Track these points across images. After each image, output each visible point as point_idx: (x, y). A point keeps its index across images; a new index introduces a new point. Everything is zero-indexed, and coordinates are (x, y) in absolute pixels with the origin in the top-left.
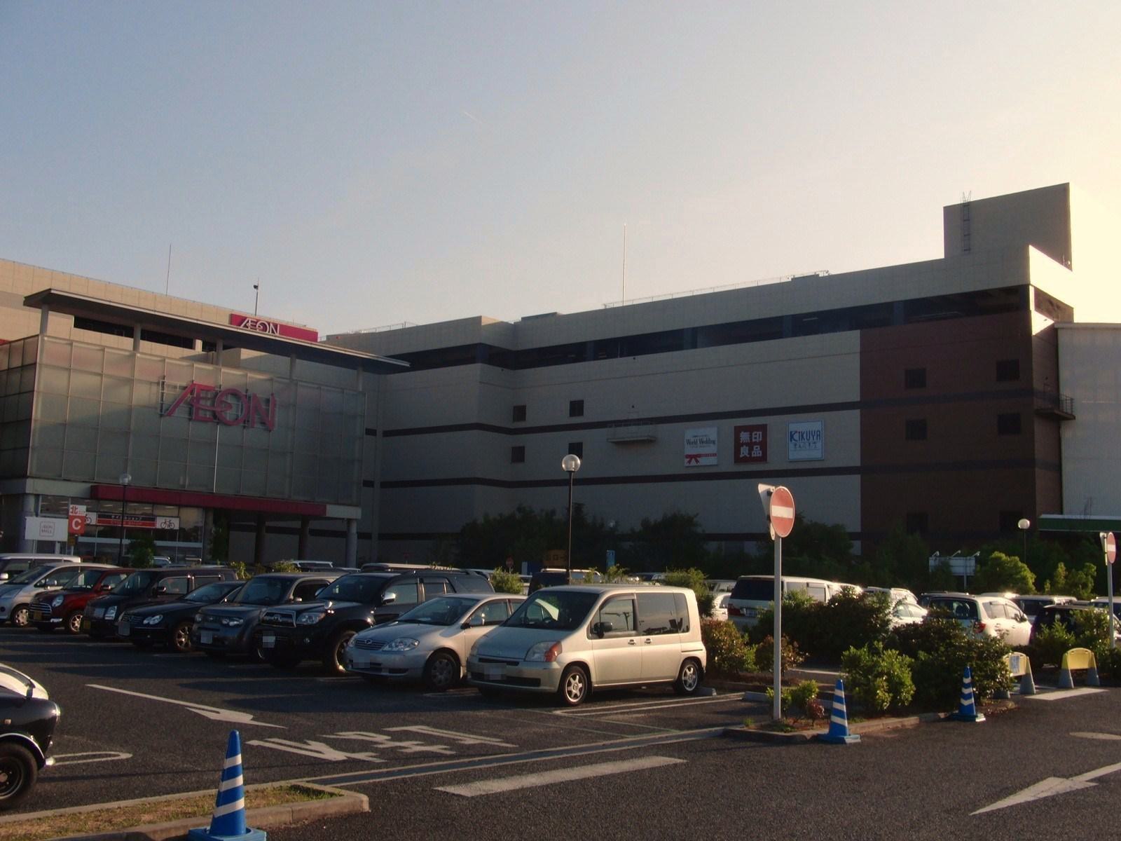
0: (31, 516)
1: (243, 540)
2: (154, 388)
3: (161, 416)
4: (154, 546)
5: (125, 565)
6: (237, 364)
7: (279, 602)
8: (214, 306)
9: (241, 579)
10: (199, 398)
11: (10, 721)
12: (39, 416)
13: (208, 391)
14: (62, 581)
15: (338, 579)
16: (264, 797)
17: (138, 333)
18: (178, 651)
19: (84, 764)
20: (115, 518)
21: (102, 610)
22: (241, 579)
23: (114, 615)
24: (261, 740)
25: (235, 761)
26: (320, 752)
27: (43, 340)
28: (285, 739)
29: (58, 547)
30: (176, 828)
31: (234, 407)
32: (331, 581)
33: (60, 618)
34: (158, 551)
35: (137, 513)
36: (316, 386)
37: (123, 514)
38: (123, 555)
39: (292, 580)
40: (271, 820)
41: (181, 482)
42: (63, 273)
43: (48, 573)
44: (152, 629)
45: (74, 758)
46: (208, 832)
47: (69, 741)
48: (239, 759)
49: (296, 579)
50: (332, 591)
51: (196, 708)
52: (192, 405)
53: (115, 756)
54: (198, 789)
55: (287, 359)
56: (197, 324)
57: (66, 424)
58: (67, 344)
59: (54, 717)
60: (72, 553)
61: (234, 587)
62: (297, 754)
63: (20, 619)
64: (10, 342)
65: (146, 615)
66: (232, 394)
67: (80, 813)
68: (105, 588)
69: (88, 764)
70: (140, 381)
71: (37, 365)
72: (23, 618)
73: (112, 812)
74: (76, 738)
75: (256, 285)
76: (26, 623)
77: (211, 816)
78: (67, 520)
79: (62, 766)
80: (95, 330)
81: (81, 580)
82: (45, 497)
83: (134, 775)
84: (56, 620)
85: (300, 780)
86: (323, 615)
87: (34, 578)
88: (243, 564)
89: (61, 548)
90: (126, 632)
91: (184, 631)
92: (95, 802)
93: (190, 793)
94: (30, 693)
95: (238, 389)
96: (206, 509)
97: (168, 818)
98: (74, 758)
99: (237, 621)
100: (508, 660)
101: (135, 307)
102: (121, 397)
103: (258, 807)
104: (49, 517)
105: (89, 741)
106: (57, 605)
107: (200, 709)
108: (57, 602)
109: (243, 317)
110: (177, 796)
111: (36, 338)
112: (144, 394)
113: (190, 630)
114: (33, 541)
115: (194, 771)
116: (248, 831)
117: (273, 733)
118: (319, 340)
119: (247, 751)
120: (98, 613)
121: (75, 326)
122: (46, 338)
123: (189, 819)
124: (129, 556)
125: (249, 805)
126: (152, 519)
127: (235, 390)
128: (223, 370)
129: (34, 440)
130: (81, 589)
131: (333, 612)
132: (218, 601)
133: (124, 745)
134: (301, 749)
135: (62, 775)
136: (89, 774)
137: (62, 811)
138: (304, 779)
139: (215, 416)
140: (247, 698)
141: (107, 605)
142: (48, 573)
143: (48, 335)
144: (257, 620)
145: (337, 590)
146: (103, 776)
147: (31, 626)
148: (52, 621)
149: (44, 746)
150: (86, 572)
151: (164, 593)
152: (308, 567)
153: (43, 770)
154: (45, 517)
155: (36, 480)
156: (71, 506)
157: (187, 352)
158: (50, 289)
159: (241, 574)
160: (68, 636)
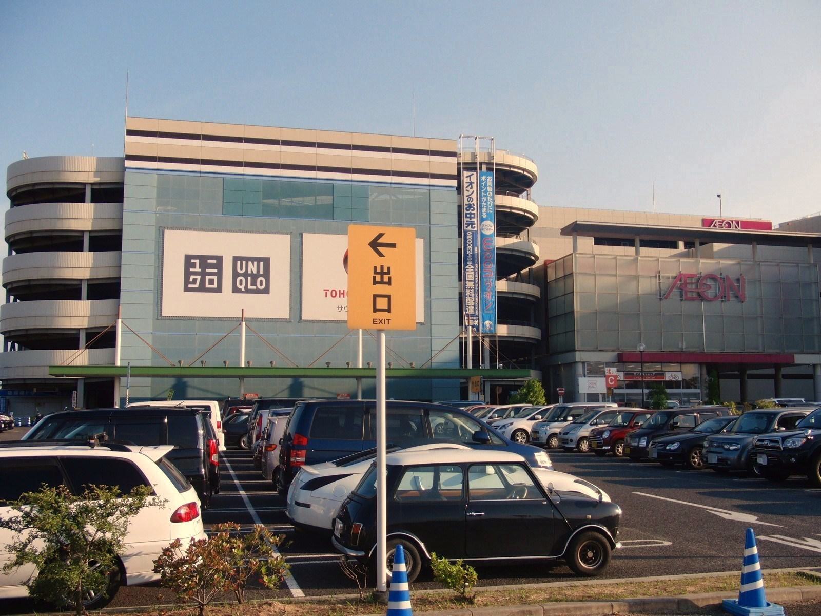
0: (582, 377)
1: (730, 386)
2: (654, 281)
3: (661, 299)
4: (665, 393)
5: (648, 408)
6: (711, 255)
7: (766, 431)
8: (689, 215)
9: (734, 415)
10: (686, 284)
11: (590, 517)
12: (579, 309)
13: (692, 277)
14: (607, 421)
15: (813, 412)
16: (777, 580)
17: (638, 242)
18: (694, 468)
19: (640, 548)
20: (636, 375)
21: (637, 440)
22: (734, 415)
23: (645, 443)
24: (767, 536)
25: (752, 551)
26: (817, 548)
27: (576, 257)
28: (786, 536)
29: (600, 396)
30: (713, 598)
31: (713, 287)
32: (808, 413)
33: (609, 446)
34: (670, 397)
35: (651, 370)
36: (776, 264)
37: (642, 371)
38: (645, 401)
39: (775, 414)
40: (785, 598)
41: (680, 346)
42: (583, 209)
43: (597, 416)
44: (673, 453)
45: (632, 544)
46: (737, 603)
47: (627, 531)
48: (755, 550)
49: (778, 413)
50: (809, 420)
51: (713, 510)
52: (682, 289)
53: (660, 543)
54: (724, 570)
55: (751, 246)
56: (649, 228)
57: (638, 315)
58: (775, 265)
59: (618, 515)
60: (611, 401)
61: (730, 420)
62: (798, 548)
63: (583, 447)
64: (555, 261)
65: (667, 443)
66: (710, 278)
67: (643, 582)
68: (636, 424)
69: (643, 548)
70: (643, 277)
71: (574, 274)
72: (585, 446)
73: (665, 583)
74: (632, 530)
75: (719, 194)
76: (587, 450)
77: (739, 592)
78: (605, 378)
79: (625, 548)
80: (608, 245)
81: (619, 420)
82: (589, 363)
83: (676, 557)
84: (606, 448)
85: (804, 568)
86: (804, 440)
87: (589, 419)
88: (734, 403)
89: (603, 398)
90: (655, 455)
91: (696, 453)
92: (651, 575)
93: (718, 573)
94: (601, 498)
95: (713, 273)
96: (701, 364)
97: (706, 591)
98: (632, 544)
99: (735, 446)
100: (369, 456)
101: (665, 226)
102: (631, 289)
103: (773, 587)
104: (592, 377)
105: (641, 532)
106: (606, 437)
107: (716, 511)
108: (606, 435)
109: (710, 220)
110: (709, 574)
111: (571, 256)
112: (647, 286)
113: (700, 453)
114: (584, 394)
115: (719, 557)
116: (768, 605)
117: (775, 531)
118: (773, 228)
119: (759, 543)
120: (634, 442)
121: (595, 244)
122: (577, 255)
123: (722, 592)
124: (649, 401)
125: (766, 585)
126: (662, 374)
127: (712, 275)
128: (702, 261)
129: (577, 326)
130: (620, 426)
131: (812, 438)
132: (719, 432)
133: (665, 536)
134: (800, 544)
135: (627, 555)
136: (644, 555)
137: (630, 579)
138: (807, 568)
139: (699, 295)
140: (751, 504)
141: (639, 436)
142: (597, 416)
143: (578, 252)
144: (751, 445)
145: (813, 420)
146: (654, 557)
147: (590, 452)
148: (604, 448)
149: (614, 534)
150: (622, 413)
151: (678, 427)
152: (785, 403)
153: (614, 550)
154: (589, 377)
155: (581, 352)
156: (606, 368)
157: (673, 251)
158: (576, 221)
159: (733, 412)
160: (615, 458)
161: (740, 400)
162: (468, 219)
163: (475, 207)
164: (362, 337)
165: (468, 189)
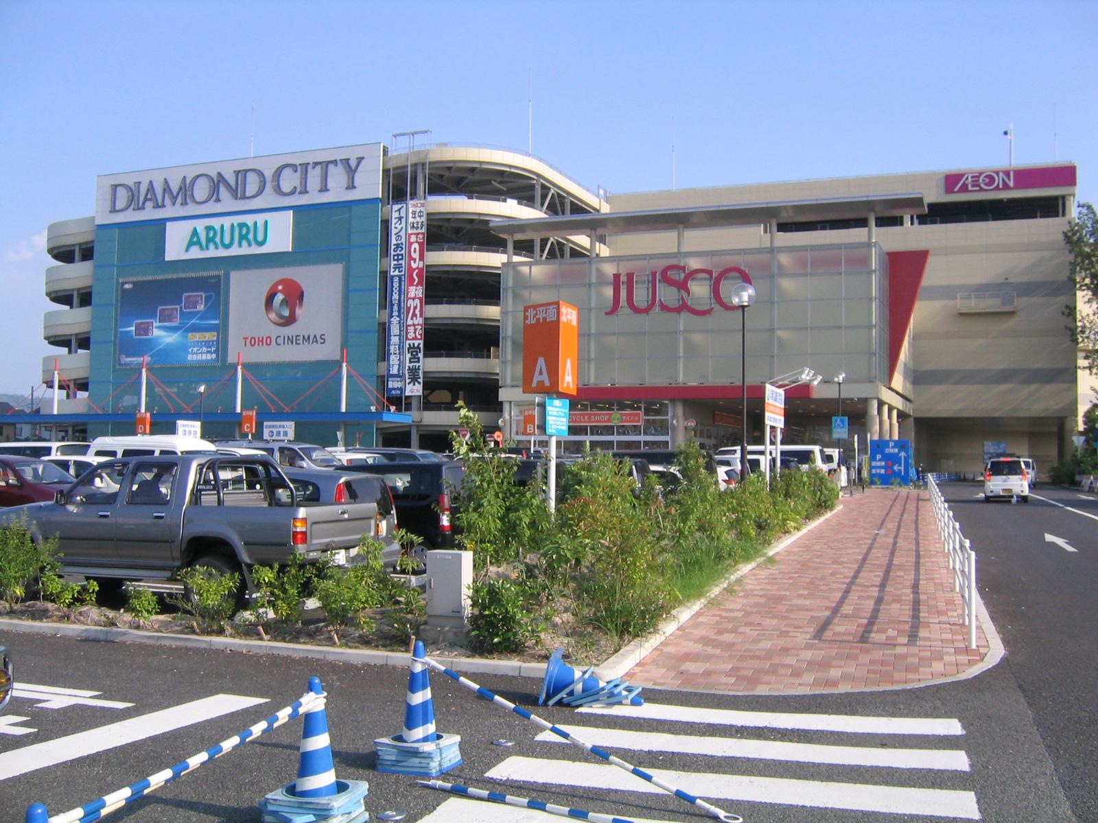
161: (548, 408)
162: (396, 262)
163: (404, 246)
164: (976, 633)
165: (397, 225)
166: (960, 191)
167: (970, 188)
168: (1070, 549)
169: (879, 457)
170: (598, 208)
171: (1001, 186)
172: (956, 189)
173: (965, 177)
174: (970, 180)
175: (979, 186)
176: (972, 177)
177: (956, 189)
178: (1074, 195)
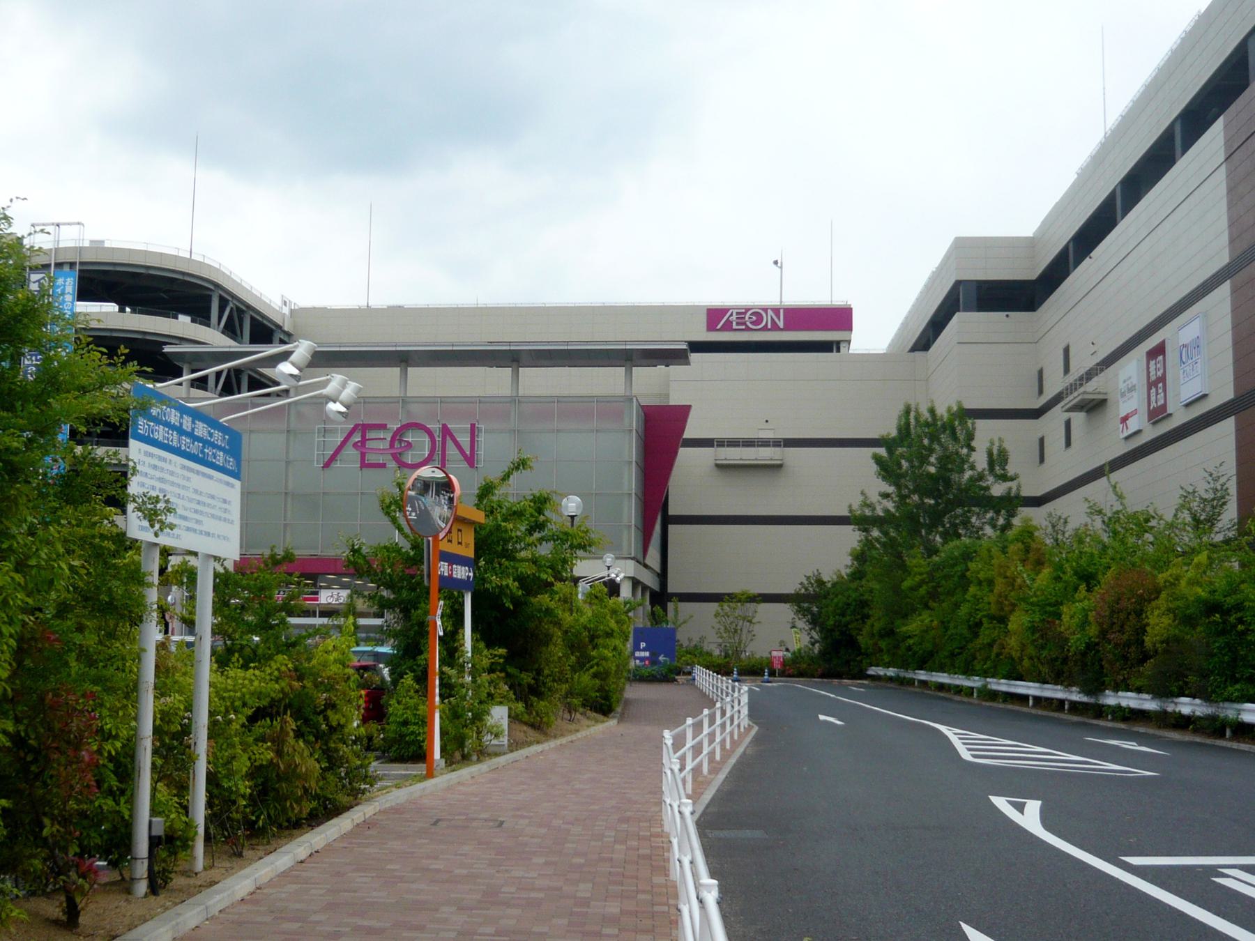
166: (723, 329)
167: (735, 326)
168: (839, 723)
169: (643, 645)
170: (281, 324)
171: (769, 326)
172: (719, 327)
173: (731, 311)
174: (735, 316)
175: (744, 324)
176: (737, 313)
177: (719, 327)
178: (849, 342)
